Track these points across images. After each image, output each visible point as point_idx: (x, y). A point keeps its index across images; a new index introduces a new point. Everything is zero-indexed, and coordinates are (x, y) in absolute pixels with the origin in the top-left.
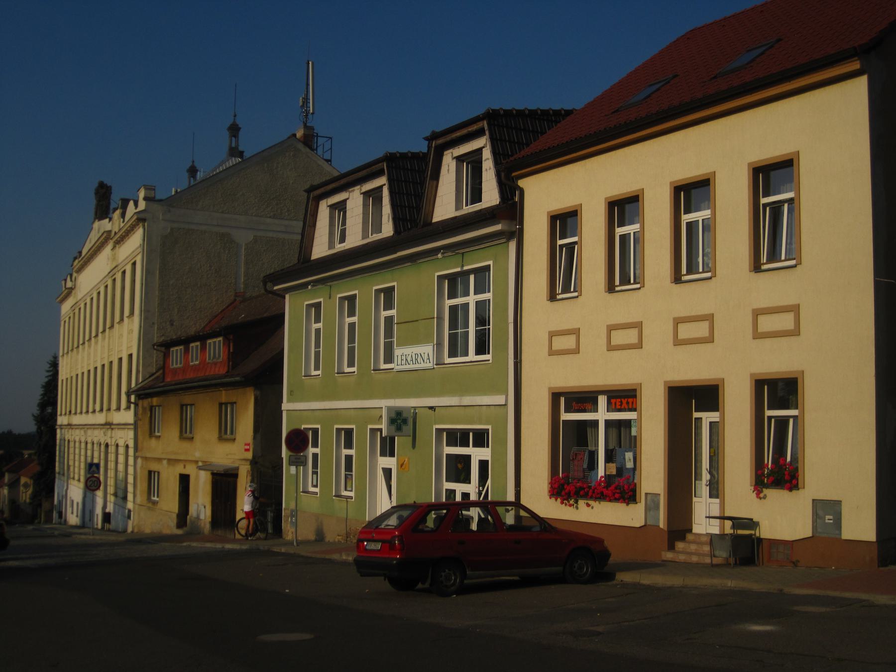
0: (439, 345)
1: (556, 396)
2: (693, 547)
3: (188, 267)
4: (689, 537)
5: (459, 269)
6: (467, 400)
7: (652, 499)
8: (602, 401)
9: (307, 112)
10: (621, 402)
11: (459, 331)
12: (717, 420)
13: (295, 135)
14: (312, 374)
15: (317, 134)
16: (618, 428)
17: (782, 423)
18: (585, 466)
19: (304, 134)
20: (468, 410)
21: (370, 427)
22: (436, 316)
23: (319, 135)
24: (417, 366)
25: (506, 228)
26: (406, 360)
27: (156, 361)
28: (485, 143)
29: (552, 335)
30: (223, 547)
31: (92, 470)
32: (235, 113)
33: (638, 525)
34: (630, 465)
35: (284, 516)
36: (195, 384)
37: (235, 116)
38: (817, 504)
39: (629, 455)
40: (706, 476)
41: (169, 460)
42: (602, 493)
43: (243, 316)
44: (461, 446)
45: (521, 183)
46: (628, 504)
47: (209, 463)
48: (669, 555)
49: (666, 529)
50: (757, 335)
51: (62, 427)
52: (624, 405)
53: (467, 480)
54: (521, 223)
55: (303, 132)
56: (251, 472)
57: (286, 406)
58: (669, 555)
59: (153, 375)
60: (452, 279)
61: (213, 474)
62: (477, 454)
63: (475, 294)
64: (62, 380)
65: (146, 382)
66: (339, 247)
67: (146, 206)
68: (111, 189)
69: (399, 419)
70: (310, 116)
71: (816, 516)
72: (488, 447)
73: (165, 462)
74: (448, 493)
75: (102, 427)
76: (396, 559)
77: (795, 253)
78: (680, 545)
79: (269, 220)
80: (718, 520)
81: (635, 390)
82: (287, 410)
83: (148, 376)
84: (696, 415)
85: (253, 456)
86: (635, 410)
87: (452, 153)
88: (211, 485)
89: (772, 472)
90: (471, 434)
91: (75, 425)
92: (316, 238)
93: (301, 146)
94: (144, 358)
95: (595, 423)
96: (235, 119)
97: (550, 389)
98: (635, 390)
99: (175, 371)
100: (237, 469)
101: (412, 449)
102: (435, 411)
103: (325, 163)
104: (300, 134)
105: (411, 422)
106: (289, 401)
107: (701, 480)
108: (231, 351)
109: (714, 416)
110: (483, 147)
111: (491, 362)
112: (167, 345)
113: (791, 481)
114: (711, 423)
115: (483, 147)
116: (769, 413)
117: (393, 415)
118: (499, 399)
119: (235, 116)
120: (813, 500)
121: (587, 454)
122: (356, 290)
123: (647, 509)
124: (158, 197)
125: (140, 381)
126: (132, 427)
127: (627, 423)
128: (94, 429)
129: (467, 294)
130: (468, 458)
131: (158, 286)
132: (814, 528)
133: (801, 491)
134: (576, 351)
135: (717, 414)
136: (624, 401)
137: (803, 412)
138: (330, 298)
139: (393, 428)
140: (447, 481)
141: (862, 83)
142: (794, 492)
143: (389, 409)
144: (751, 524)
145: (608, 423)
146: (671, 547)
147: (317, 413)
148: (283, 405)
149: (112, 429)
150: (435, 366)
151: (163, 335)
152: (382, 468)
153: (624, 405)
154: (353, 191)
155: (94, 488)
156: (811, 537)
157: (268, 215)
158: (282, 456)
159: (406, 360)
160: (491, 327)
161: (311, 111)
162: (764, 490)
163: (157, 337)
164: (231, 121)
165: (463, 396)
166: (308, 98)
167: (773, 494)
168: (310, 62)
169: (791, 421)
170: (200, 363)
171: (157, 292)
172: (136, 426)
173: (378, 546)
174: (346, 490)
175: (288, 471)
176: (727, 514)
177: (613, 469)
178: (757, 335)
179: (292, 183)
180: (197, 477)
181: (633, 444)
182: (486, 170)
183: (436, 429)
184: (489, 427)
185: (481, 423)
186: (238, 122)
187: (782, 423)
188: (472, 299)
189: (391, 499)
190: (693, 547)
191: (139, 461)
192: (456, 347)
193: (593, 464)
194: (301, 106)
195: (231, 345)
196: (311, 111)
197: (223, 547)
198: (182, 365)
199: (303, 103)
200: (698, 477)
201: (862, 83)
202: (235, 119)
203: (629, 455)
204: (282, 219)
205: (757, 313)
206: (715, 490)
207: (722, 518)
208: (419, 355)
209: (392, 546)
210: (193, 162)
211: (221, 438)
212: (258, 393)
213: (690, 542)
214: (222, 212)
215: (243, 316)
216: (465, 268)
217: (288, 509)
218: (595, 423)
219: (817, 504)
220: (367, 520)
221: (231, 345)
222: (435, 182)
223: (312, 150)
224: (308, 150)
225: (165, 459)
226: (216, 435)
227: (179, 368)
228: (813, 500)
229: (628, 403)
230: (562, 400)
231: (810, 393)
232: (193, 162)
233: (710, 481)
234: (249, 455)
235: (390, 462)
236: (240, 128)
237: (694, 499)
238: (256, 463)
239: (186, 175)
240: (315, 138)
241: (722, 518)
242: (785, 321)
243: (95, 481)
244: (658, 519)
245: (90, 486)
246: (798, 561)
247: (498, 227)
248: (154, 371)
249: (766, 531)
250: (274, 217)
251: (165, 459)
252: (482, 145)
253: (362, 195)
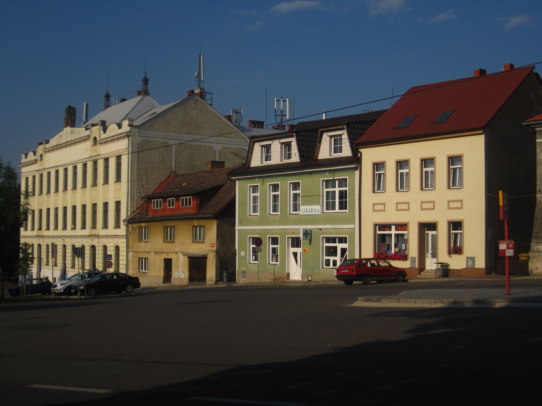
0: (323, 206)
1: (375, 225)
2: (427, 274)
3: (149, 159)
4: (425, 271)
5: (332, 178)
6: (337, 226)
7: (413, 259)
8: (393, 228)
9: (200, 81)
10: (401, 228)
11: (331, 201)
12: (436, 234)
13: (193, 92)
14: (251, 215)
15: (205, 92)
17: (456, 235)
18: (386, 249)
19: (200, 92)
20: (337, 230)
21: (248, 236)
22: (321, 195)
23: (206, 92)
24: (312, 213)
25: (355, 166)
26: (307, 211)
27: (136, 205)
28: (343, 132)
29: (374, 205)
30: (217, 286)
31: (108, 258)
32: (146, 71)
34: (404, 248)
35: (237, 274)
36: (189, 217)
37: (146, 73)
38: (468, 258)
39: (403, 245)
40: (430, 251)
41: (156, 253)
42: (395, 258)
43: (185, 184)
46: (404, 261)
47: (186, 253)
48: (419, 276)
49: (418, 268)
50: (449, 208)
51: (99, 237)
52: (402, 228)
53: (336, 255)
54: (361, 165)
55: (199, 91)
56: (216, 256)
57: (237, 227)
58: (419, 276)
59: (135, 212)
60: (327, 181)
61: (189, 258)
62: (340, 246)
65: (134, 214)
66: (266, 163)
67: (130, 129)
68: (76, 110)
69: (307, 233)
70: (201, 82)
71: (467, 262)
72: (300, 247)
73: (152, 253)
74: (326, 260)
75: (36, 237)
76: (355, 274)
77: (461, 184)
78: (422, 273)
79: (185, 135)
80: (436, 264)
81: (407, 224)
82: (238, 229)
83: (132, 212)
84: (427, 232)
85: (217, 249)
86: (407, 230)
87: (327, 134)
89: (453, 249)
90: (337, 239)
92: (253, 158)
93: (198, 97)
94: (131, 204)
95: (390, 235)
96: (145, 75)
97: (373, 223)
98: (407, 224)
100: (207, 255)
101: (309, 245)
102: (321, 230)
103: (209, 105)
104: (197, 91)
105: (310, 234)
106: (239, 225)
107: (428, 252)
108: (198, 203)
109: (434, 233)
110: (343, 134)
111: (347, 213)
112: (149, 199)
113: (460, 252)
114: (432, 235)
115: (343, 134)
116: (452, 232)
118: (352, 226)
119: (146, 73)
120: (467, 257)
121: (386, 245)
122: (279, 182)
123: (411, 262)
125: (129, 215)
126: (125, 237)
127: (403, 235)
128: (56, 238)
129: (334, 187)
130: (335, 248)
131: (136, 168)
133: (463, 255)
134: (384, 210)
135: (436, 232)
136: (402, 227)
137: (463, 231)
138: (263, 184)
140: (326, 256)
141: (483, 136)
142: (461, 255)
143: (303, 229)
144: (448, 265)
145: (396, 235)
146: (420, 274)
147: (257, 231)
148: (236, 228)
149: (99, 238)
150: (321, 214)
151: (139, 192)
152: (292, 252)
153: (402, 228)
154: (275, 141)
155: (110, 267)
156: (465, 268)
157: (185, 133)
158: (236, 249)
159: (307, 211)
160: (347, 200)
161: (202, 80)
162: (451, 255)
163: (136, 193)
164: (143, 76)
165: (334, 225)
166: (201, 73)
167: (454, 256)
168: (202, 55)
169: (459, 234)
170: (175, 208)
171: (136, 172)
174: (272, 261)
176: (439, 262)
177: (397, 250)
178: (449, 208)
179: (195, 117)
180: (178, 259)
181: (406, 241)
182: (344, 143)
183: (322, 237)
184: (278, 236)
186: (148, 76)
187: (456, 235)
188: (337, 190)
189: (297, 264)
190: (427, 274)
192: (330, 206)
193: (389, 248)
194: (196, 77)
195: (198, 200)
196: (202, 80)
197: (217, 286)
199: (198, 75)
200: (428, 251)
201: (483, 136)
202: (145, 75)
203: (403, 245)
204: (191, 134)
205: (449, 202)
207: (438, 263)
208: (313, 209)
209: (353, 271)
210: (107, 91)
211: (193, 242)
212: (218, 221)
213: (426, 272)
214: (164, 132)
215: (185, 184)
216: (335, 178)
217: (240, 271)
218: (390, 235)
219: (468, 258)
220: (286, 272)
221: (198, 200)
222: (320, 144)
223: (203, 99)
224: (202, 100)
225: (152, 252)
226: (191, 240)
228: (467, 257)
229: (403, 228)
230: (377, 227)
231: (465, 226)
232: (107, 91)
233: (432, 253)
234: (215, 249)
235: (299, 250)
236: (148, 80)
237: (426, 259)
238: (218, 252)
239: (104, 99)
240: (204, 93)
241: (438, 263)
243: (110, 263)
244: (415, 265)
245: (108, 266)
246: (462, 275)
247: (353, 166)
248: (135, 210)
249: (451, 267)
250: (187, 134)
252: (342, 133)
253: (280, 144)
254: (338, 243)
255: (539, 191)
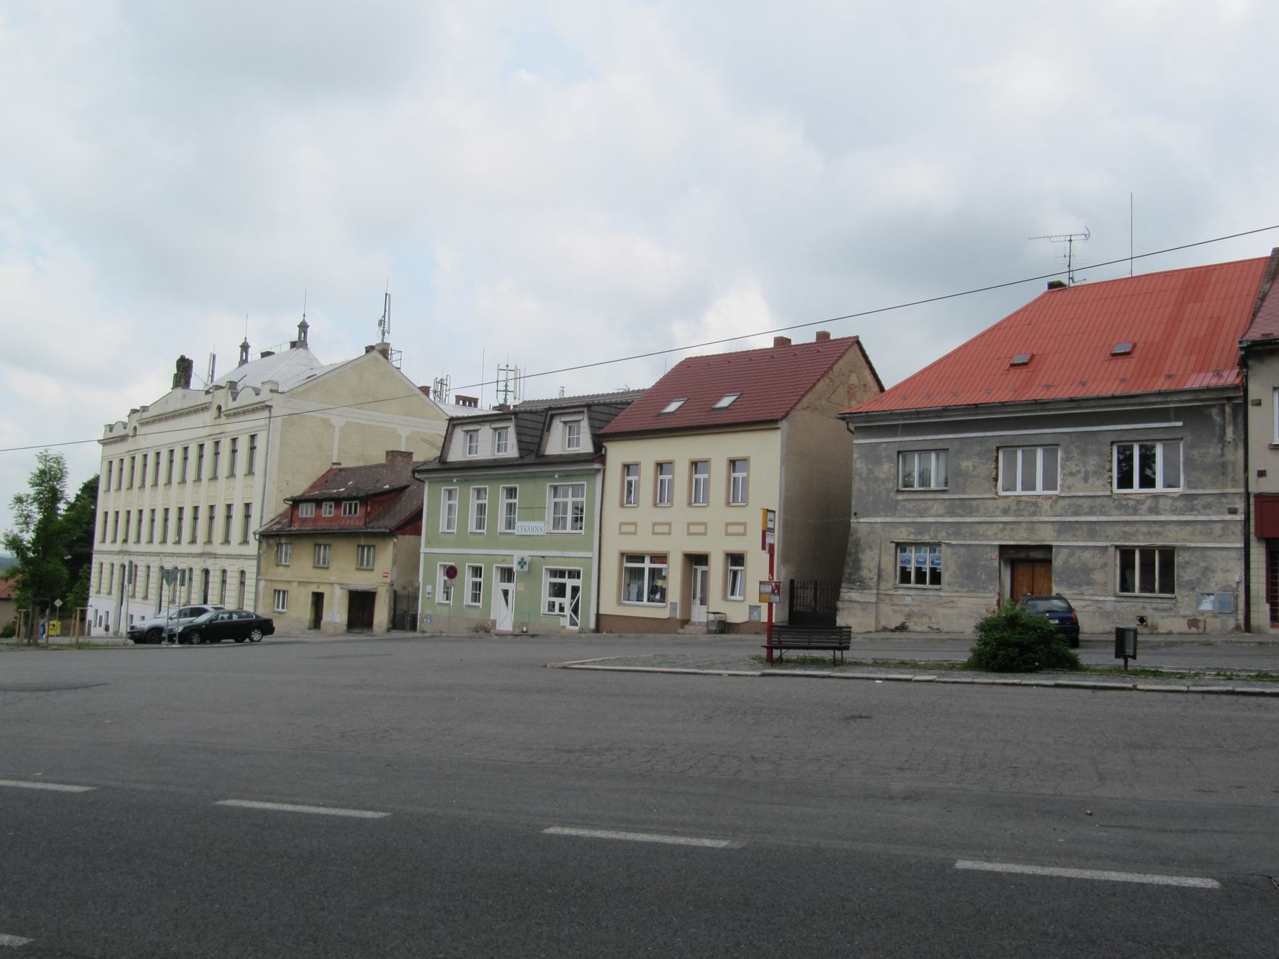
4: (691, 623)
7: (673, 604)
16: (655, 573)
17: (735, 573)
33: (666, 617)
41: (300, 583)
44: (560, 577)
45: (604, 444)
53: (564, 596)
62: (570, 583)
63: (572, 497)
64: (106, 513)
88: (348, 600)
91: (220, 555)
99: (304, 520)
117: (520, 560)
123: (671, 610)
124: (279, 391)
127: (660, 570)
130: (563, 586)
132: (750, 617)
137: (746, 568)
139: (520, 566)
172: (259, 557)
173: (1057, 622)
175: (424, 589)
185: (575, 566)
188: (570, 500)
191: (262, 583)
198: (313, 515)
206: (704, 601)
225: (294, 581)
227: (310, 518)
242: (740, 529)
251: (294, 581)
254: (569, 577)
255: (855, 514)
